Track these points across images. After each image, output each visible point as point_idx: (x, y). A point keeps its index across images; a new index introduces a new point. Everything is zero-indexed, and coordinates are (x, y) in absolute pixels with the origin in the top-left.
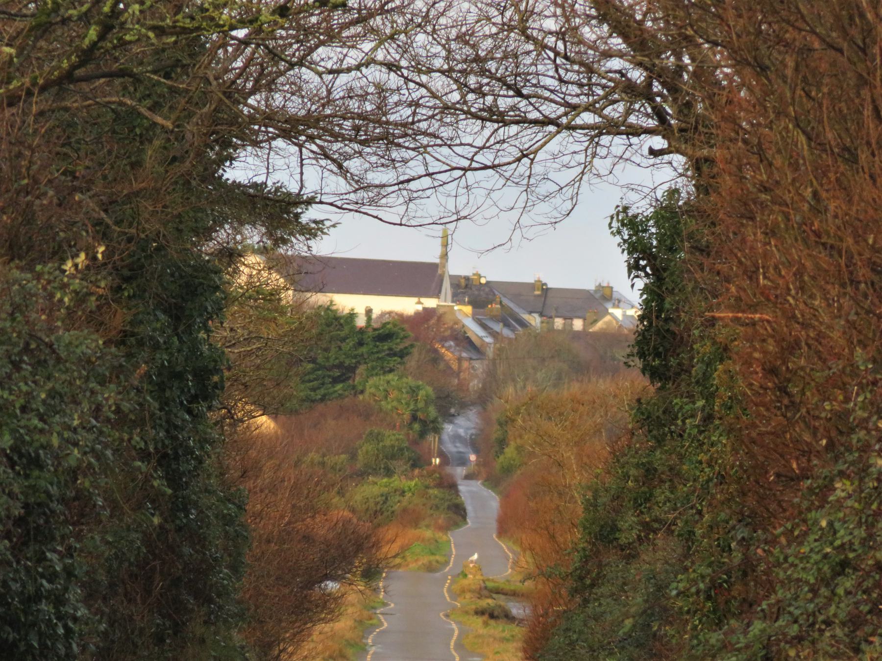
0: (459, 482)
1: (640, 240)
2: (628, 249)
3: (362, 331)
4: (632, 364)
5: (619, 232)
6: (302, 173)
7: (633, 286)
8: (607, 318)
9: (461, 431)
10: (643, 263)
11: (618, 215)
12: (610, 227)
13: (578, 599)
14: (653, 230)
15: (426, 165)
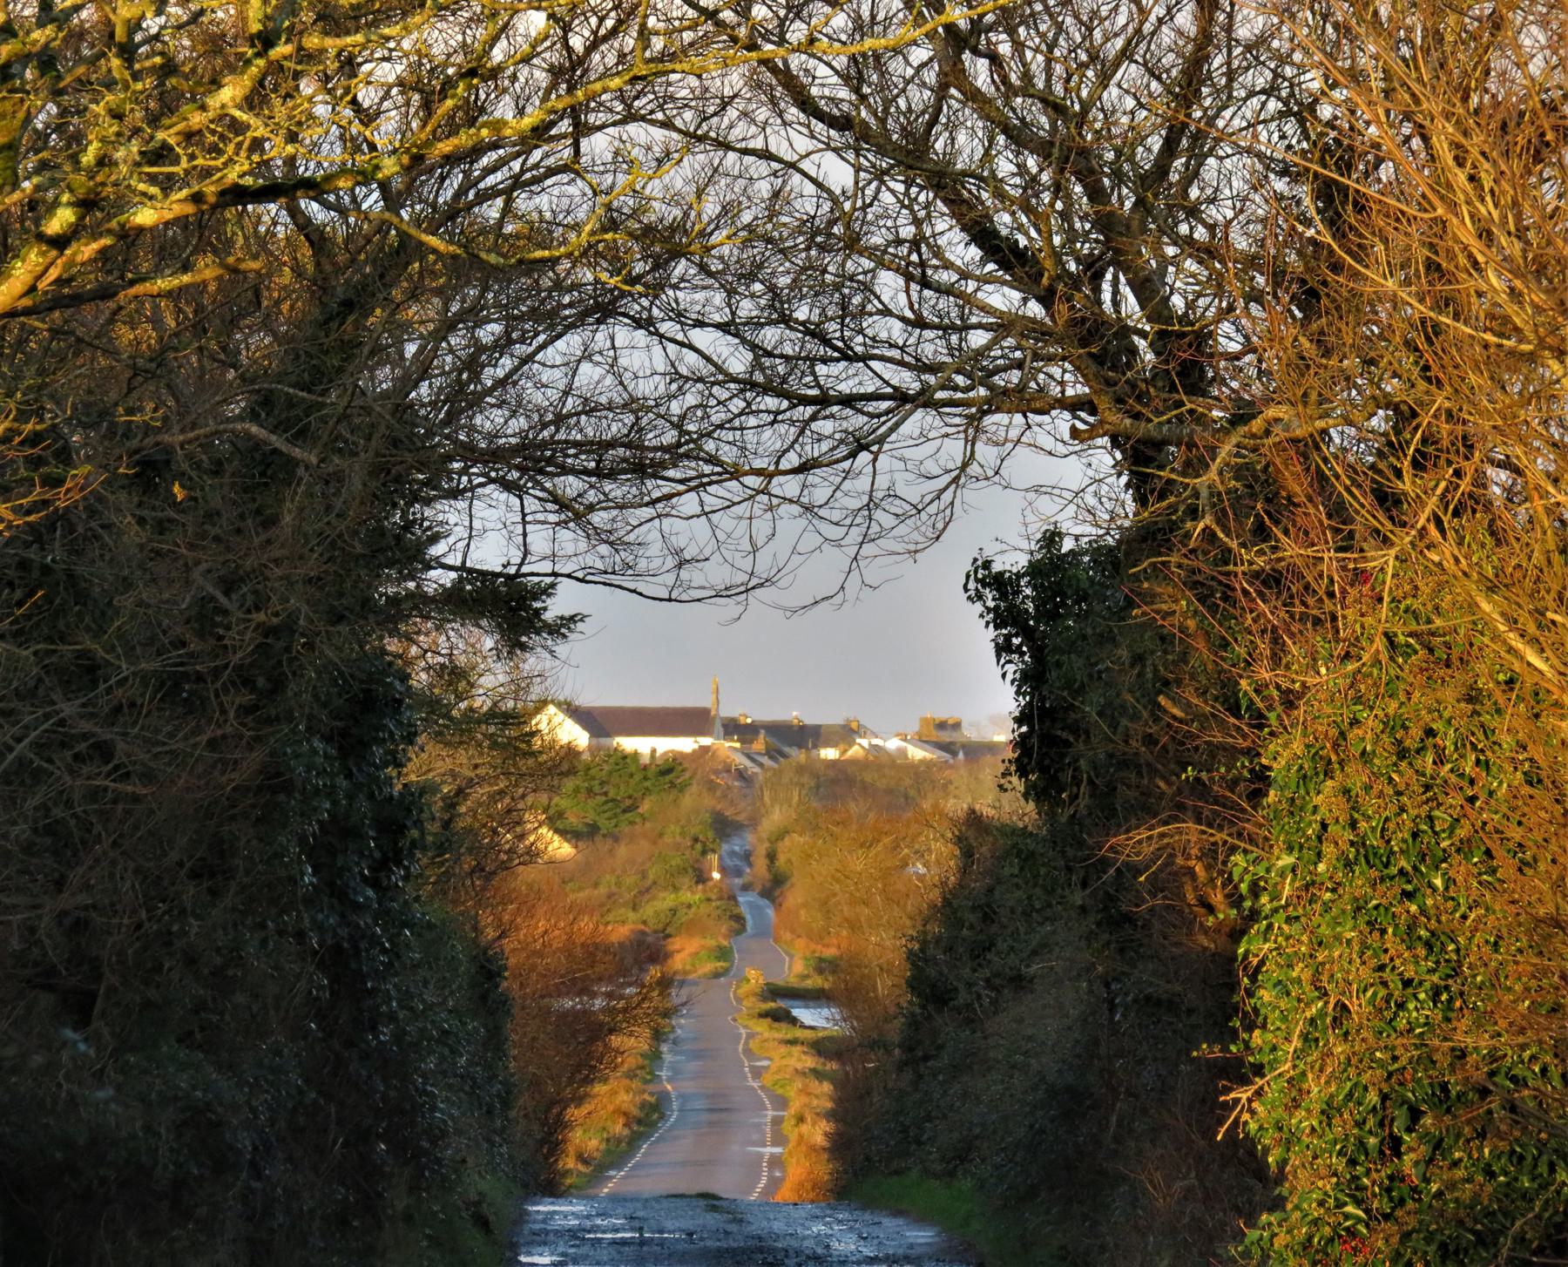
0: (738, 893)
1: (1011, 607)
2: (994, 620)
3: (645, 768)
4: (1007, 786)
5: (980, 597)
6: (525, 535)
7: (1004, 676)
8: (856, 748)
9: (737, 848)
10: (1016, 641)
11: (976, 572)
12: (966, 589)
13: (908, 1075)
14: (1028, 591)
15: (702, 503)
